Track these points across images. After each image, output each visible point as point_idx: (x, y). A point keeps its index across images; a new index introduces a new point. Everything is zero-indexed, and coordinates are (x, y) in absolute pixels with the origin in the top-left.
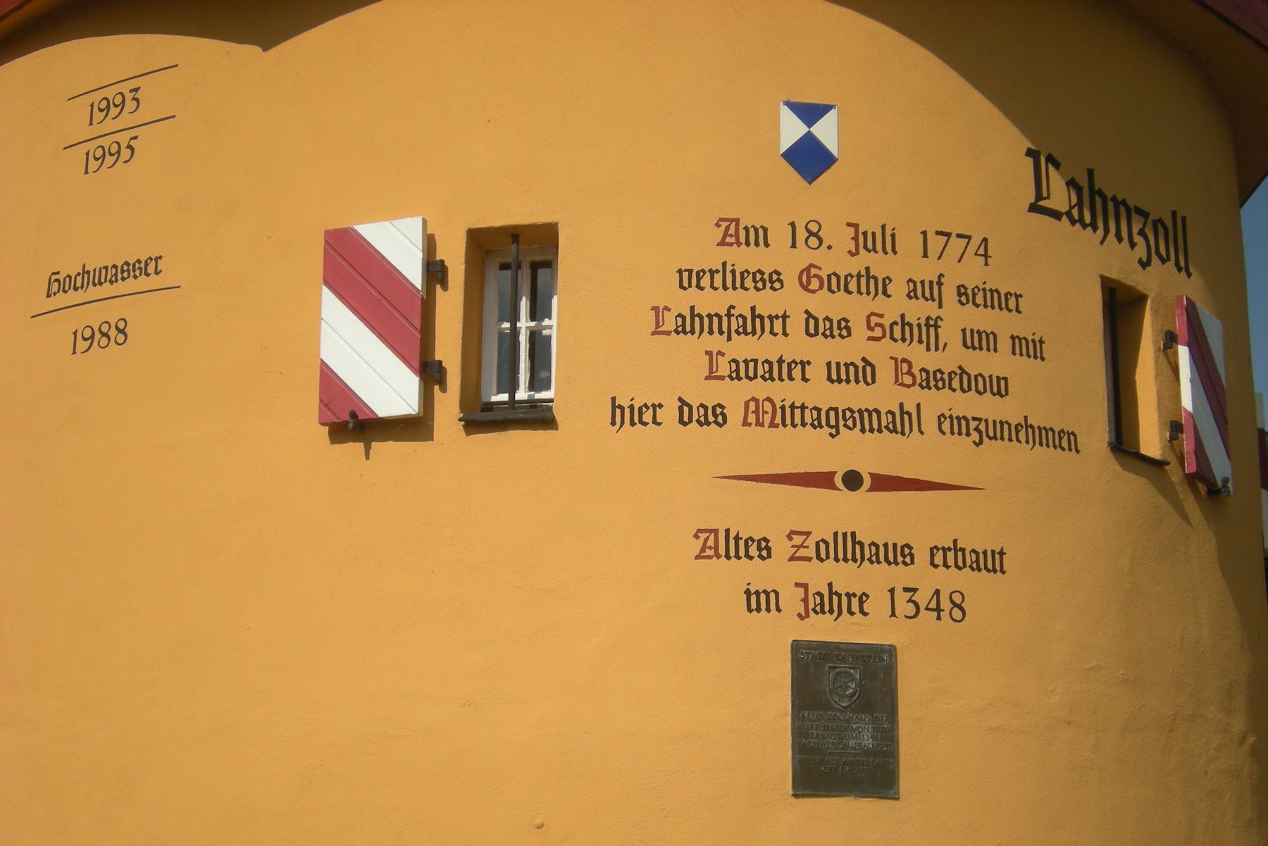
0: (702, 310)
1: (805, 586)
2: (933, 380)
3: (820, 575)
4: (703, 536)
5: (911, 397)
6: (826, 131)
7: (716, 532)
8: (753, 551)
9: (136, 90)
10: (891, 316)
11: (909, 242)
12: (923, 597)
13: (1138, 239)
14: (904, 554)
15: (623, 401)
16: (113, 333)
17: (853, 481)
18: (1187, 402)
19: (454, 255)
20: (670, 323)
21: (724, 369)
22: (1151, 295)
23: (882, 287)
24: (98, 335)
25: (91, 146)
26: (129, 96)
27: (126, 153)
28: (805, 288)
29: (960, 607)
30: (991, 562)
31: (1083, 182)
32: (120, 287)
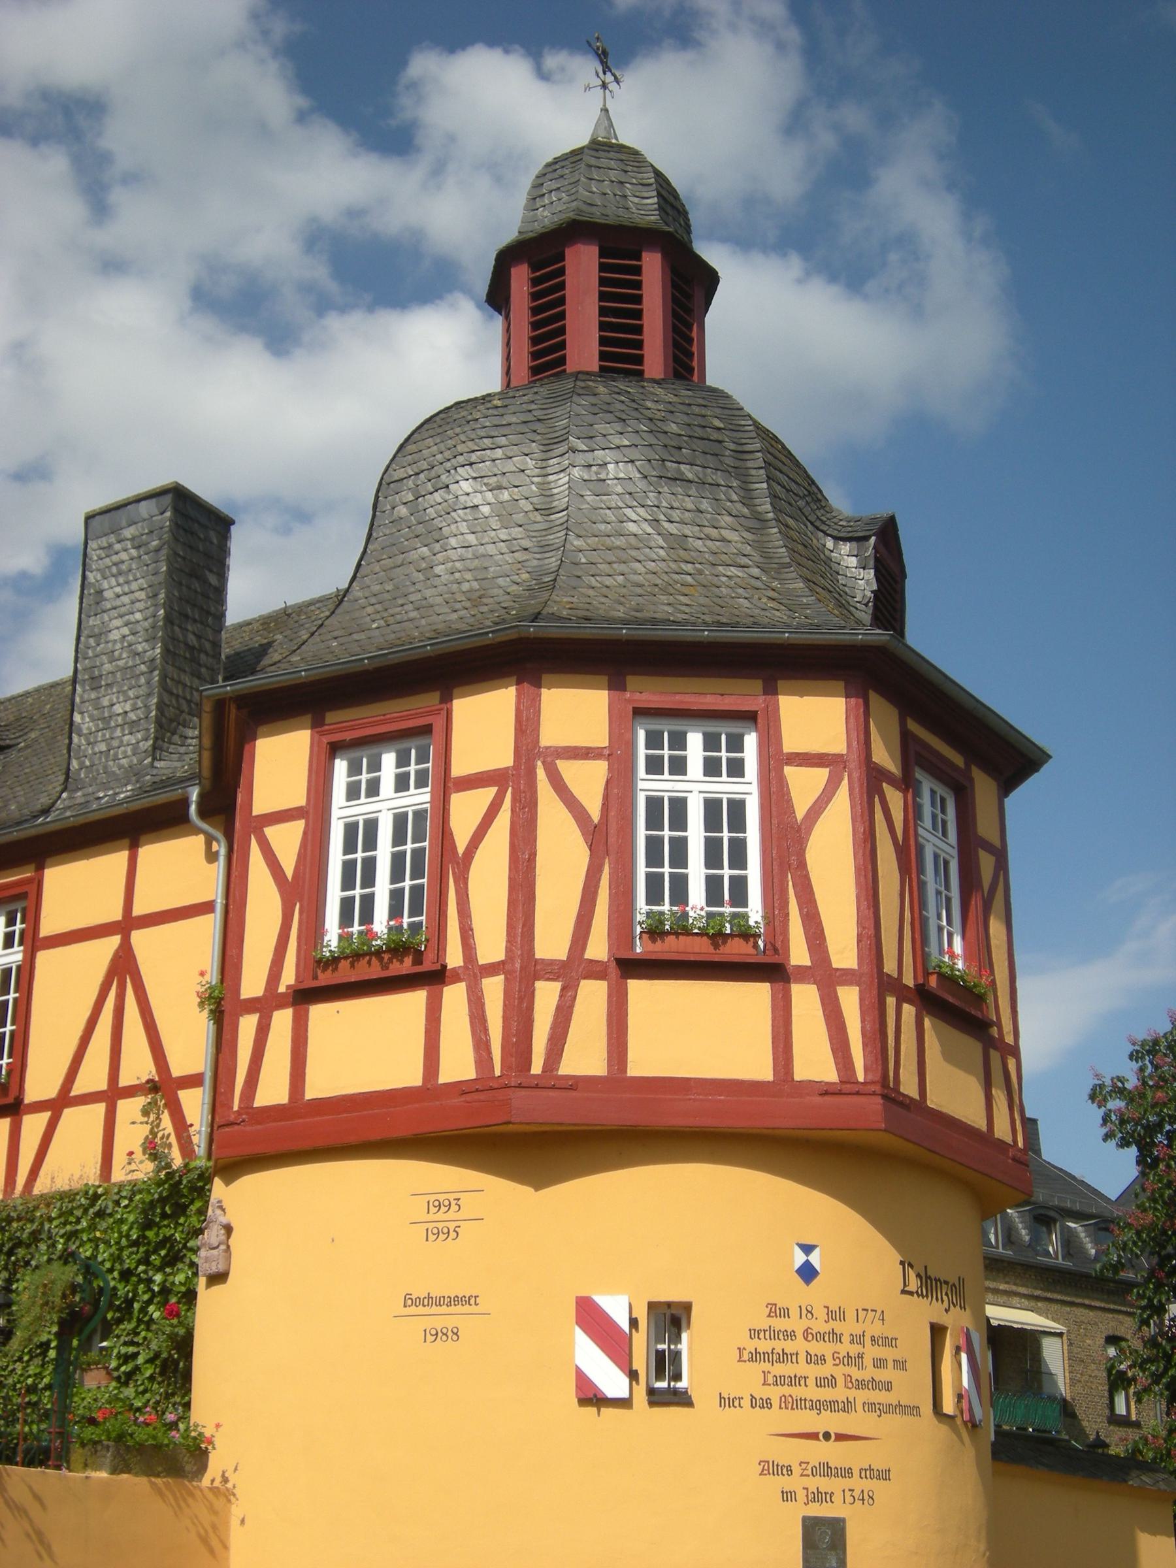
0: (760, 1350)
1: (807, 1489)
2: (861, 1385)
3: (814, 1483)
4: (762, 1464)
5: (852, 1393)
6: (815, 1259)
7: (768, 1462)
8: (785, 1471)
9: (459, 1199)
10: (843, 1353)
11: (850, 1315)
12: (857, 1494)
13: (945, 1298)
14: (847, 1473)
15: (725, 1395)
16: (450, 1334)
17: (827, 1436)
18: (965, 1383)
19: (642, 1315)
20: (746, 1356)
21: (770, 1380)
22: (950, 1327)
23: (839, 1338)
24: (440, 1334)
25: (430, 1226)
26: (453, 1203)
27: (453, 1235)
28: (806, 1339)
29: (811, 1312)
30: (884, 1475)
31: (923, 1274)
32: (452, 1309)
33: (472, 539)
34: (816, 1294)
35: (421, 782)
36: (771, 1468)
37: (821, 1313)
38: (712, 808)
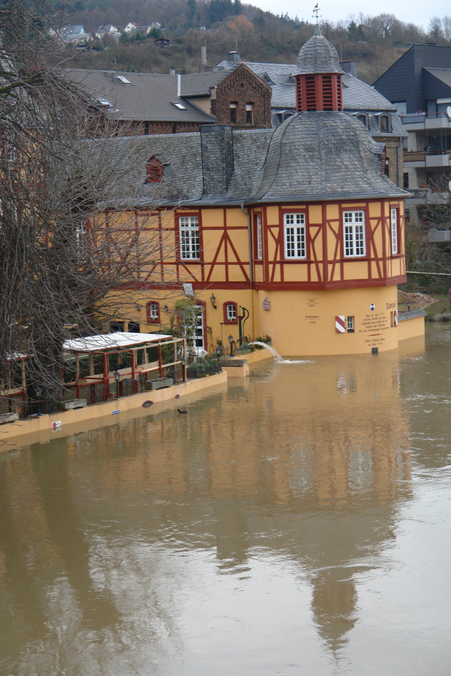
6: (374, 306)
14: (378, 340)
33: (305, 164)
34: (374, 312)
35: (302, 222)
36: (367, 341)
37: (374, 315)
38: (357, 228)
